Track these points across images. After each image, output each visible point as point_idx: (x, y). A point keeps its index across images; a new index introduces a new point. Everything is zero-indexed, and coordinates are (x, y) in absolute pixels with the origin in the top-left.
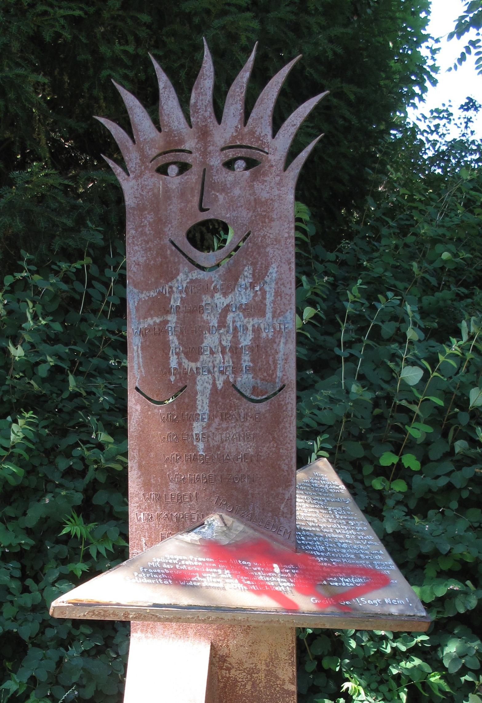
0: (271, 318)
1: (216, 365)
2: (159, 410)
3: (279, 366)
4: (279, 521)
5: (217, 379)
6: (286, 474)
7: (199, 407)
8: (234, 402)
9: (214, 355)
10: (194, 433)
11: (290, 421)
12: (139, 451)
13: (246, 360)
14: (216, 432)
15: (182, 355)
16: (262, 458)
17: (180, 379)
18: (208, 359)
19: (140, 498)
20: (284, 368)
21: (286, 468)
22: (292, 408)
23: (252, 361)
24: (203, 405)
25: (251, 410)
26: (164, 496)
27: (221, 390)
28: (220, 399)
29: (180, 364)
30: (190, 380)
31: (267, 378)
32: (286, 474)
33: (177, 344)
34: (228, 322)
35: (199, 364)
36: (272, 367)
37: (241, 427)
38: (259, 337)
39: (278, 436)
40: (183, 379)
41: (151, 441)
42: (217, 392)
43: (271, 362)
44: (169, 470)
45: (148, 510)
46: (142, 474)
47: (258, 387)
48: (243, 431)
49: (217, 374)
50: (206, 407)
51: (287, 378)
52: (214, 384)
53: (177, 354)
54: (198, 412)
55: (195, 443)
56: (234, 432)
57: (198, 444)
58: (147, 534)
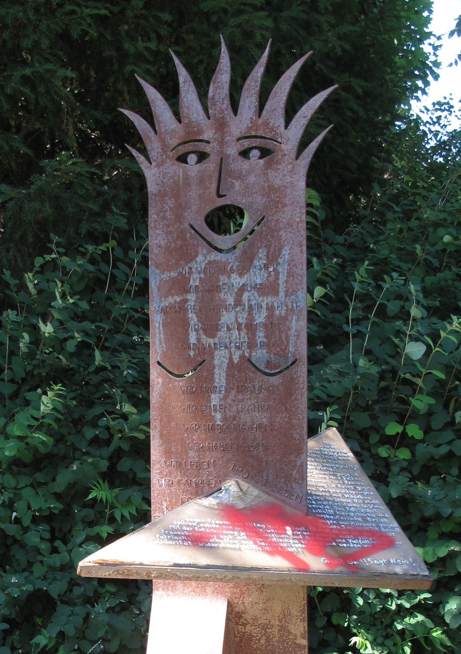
2: (179, 382)
3: (291, 342)
4: (291, 487)
5: (233, 354)
6: (298, 442)
7: (217, 380)
8: (249, 375)
10: (212, 404)
11: (302, 393)
12: (161, 421)
13: (260, 336)
14: (233, 404)
15: (201, 332)
16: (276, 428)
18: (225, 335)
19: (161, 465)
23: (266, 337)
24: (220, 378)
25: (265, 382)
26: (184, 463)
27: (237, 364)
28: (236, 373)
29: (199, 340)
30: (208, 355)
32: (298, 442)
33: (196, 321)
35: (216, 340)
36: (285, 343)
37: (255, 398)
39: (291, 407)
40: (201, 353)
41: (172, 411)
45: (169, 476)
47: (271, 362)
49: (233, 349)
50: (223, 380)
51: (299, 353)
52: (231, 359)
54: (216, 384)
55: (213, 414)
56: (250, 404)
57: (216, 414)
58: (168, 498)
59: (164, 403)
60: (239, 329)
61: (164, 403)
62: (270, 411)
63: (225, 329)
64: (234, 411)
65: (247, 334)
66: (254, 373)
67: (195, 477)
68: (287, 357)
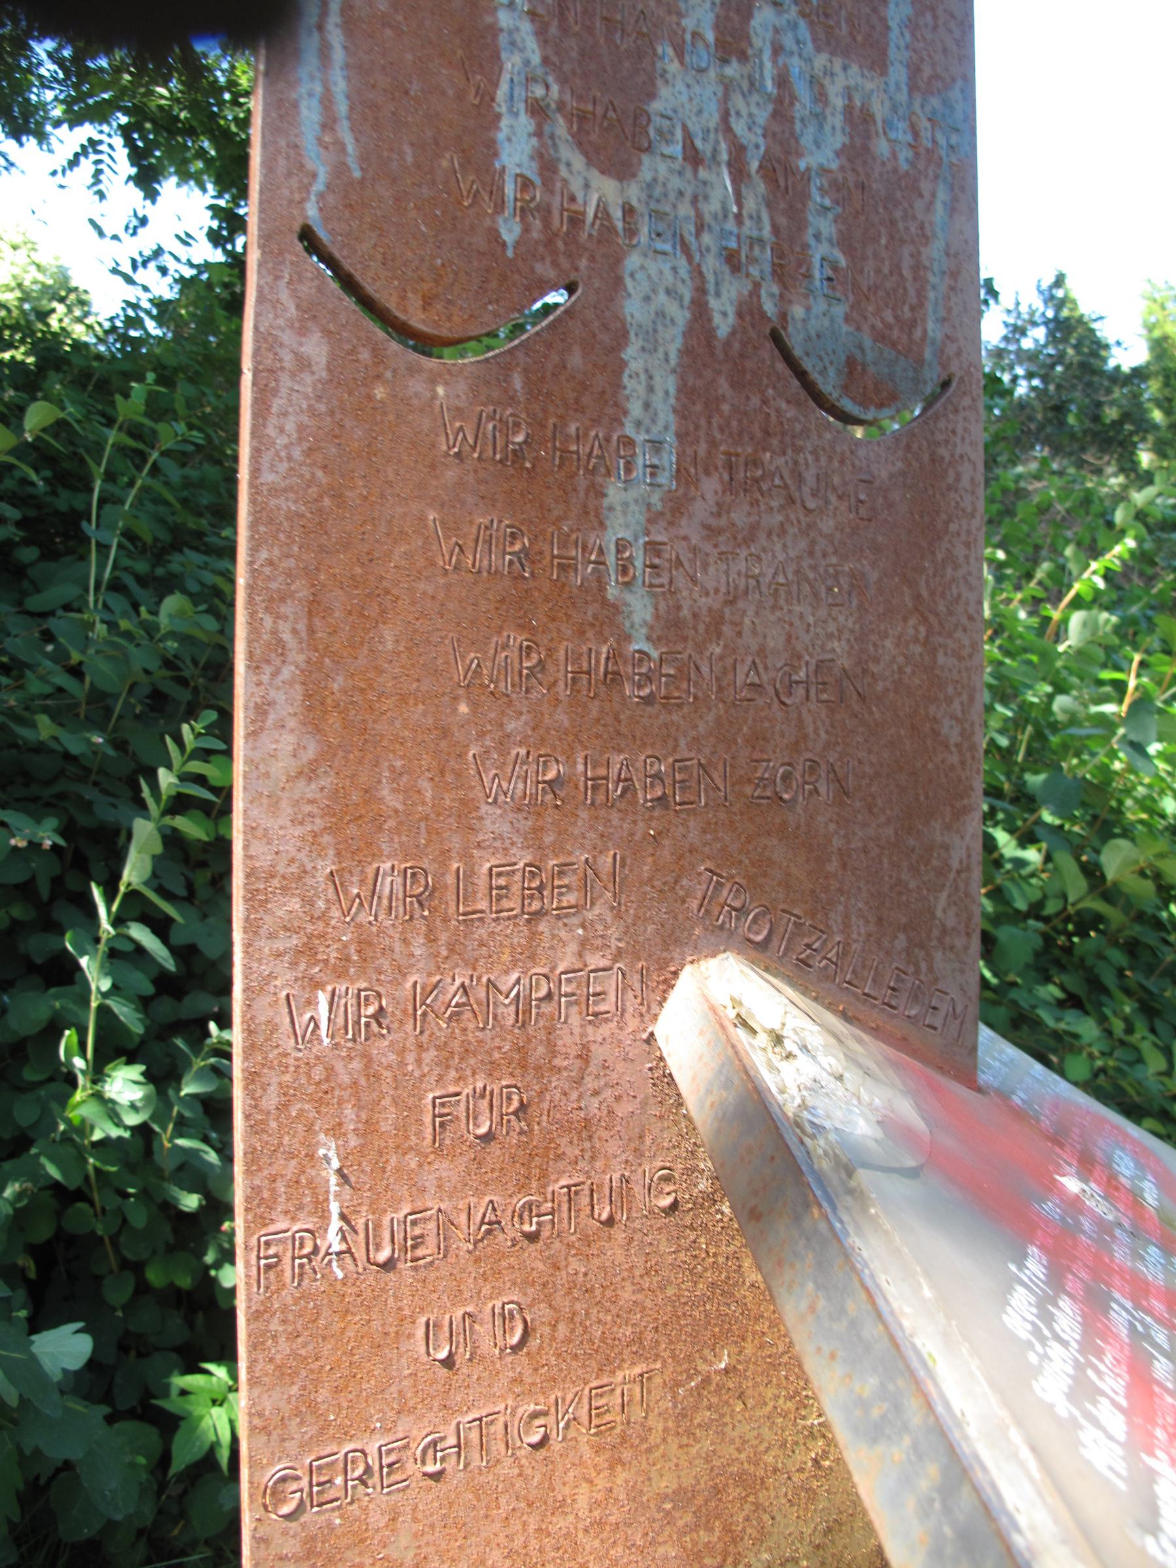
0: (905, 89)
1: (708, 218)
2: (433, 381)
3: (931, 295)
4: (931, 969)
5: (711, 287)
6: (954, 759)
7: (635, 409)
8: (778, 410)
9: (703, 173)
10: (609, 540)
11: (969, 532)
12: (315, 607)
13: (822, 228)
14: (707, 547)
15: (560, 127)
16: (880, 686)
17: (549, 243)
18: (675, 183)
19: (309, 902)
20: (949, 310)
21: (954, 737)
22: (972, 480)
23: (845, 242)
24: (650, 387)
25: (842, 462)
26: (450, 879)
27: (727, 344)
28: (723, 386)
29: (548, 165)
30: (592, 259)
31: (896, 333)
32: (954, 759)
33: (536, 59)
34: (757, 42)
35: (634, 193)
36: (912, 298)
37: (805, 532)
38: (866, 149)
39: (932, 594)
40: (560, 244)
41: (388, 555)
42: (710, 345)
43: (906, 272)
44: (481, 735)
45: (362, 971)
46: (327, 754)
47: (864, 365)
48: (811, 554)
49: (712, 264)
50: (666, 415)
51: (959, 353)
52: (700, 310)
53: (537, 110)
54: (629, 430)
55: (612, 592)
56: (781, 557)
57: (629, 597)
58: (349, 1112)
59: (338, 497)
60: (739, 174)
61: (338, 497)
62: (860, 606)
63: (677, 149)
64: (710, 586)
65: (769, 205)
66: (798, 404)
67: (514, 963)
68: (920, 362)
